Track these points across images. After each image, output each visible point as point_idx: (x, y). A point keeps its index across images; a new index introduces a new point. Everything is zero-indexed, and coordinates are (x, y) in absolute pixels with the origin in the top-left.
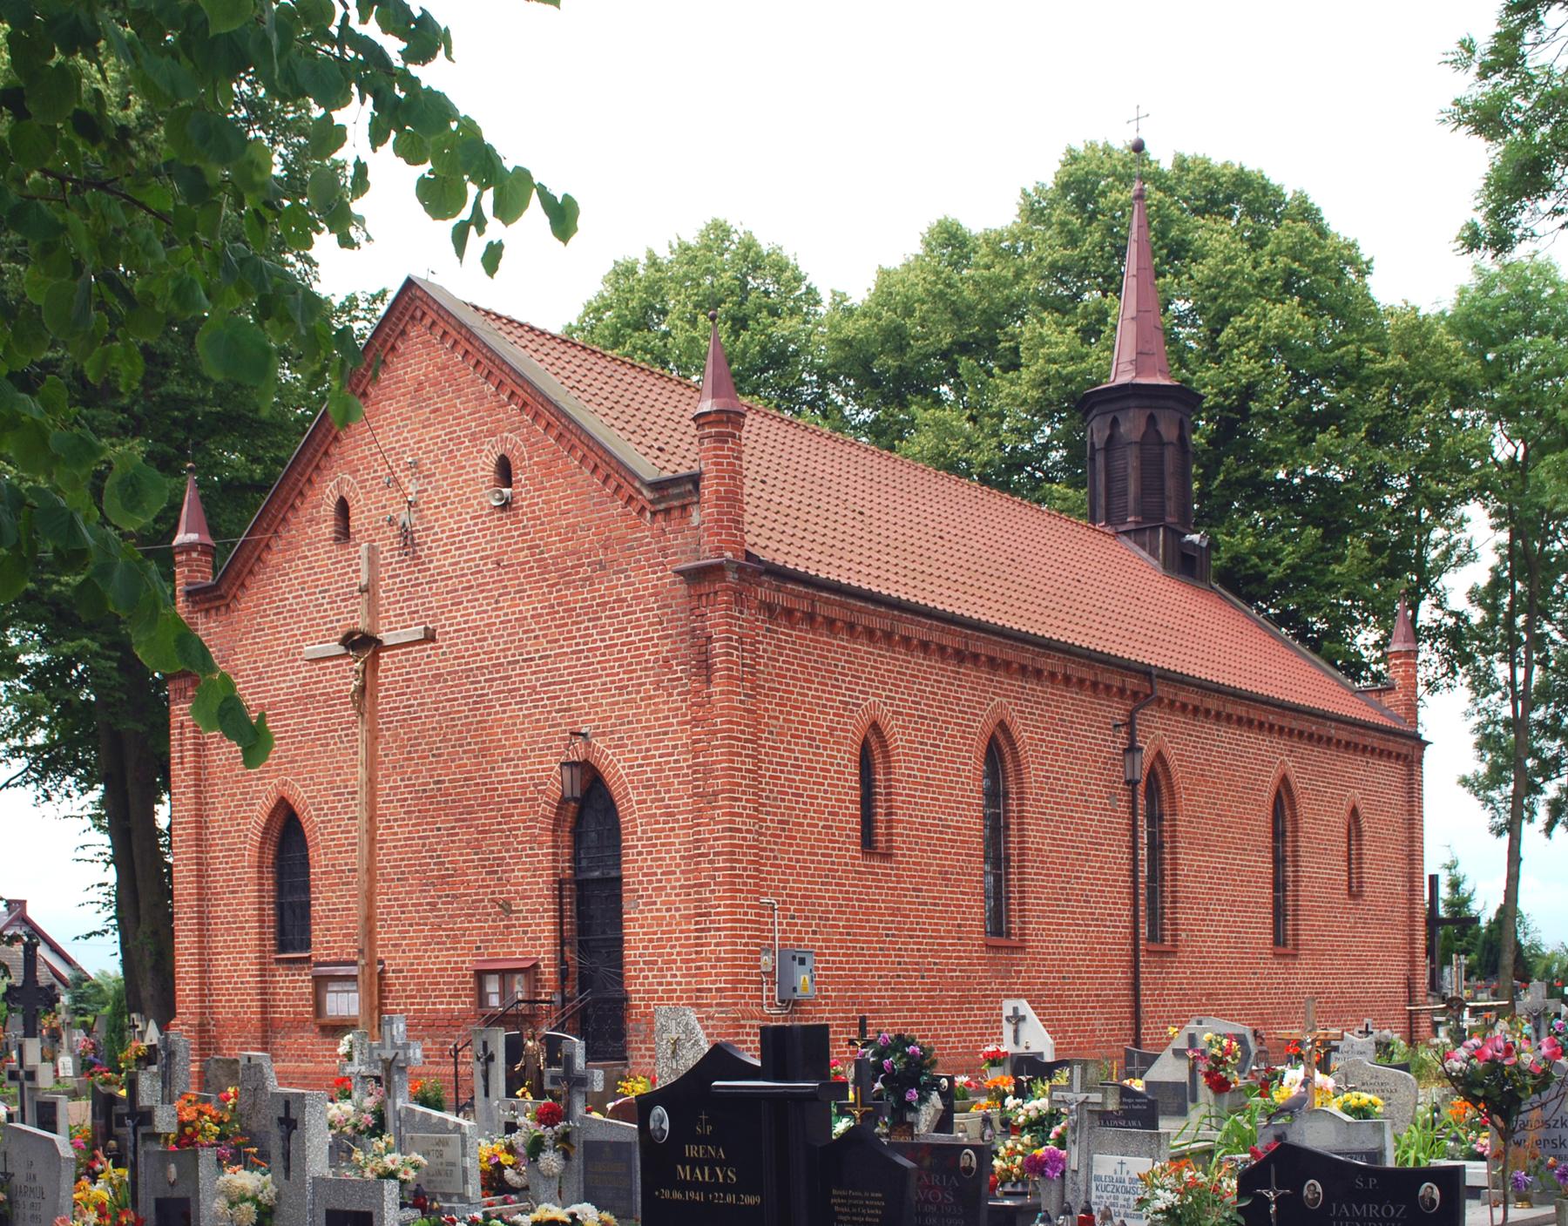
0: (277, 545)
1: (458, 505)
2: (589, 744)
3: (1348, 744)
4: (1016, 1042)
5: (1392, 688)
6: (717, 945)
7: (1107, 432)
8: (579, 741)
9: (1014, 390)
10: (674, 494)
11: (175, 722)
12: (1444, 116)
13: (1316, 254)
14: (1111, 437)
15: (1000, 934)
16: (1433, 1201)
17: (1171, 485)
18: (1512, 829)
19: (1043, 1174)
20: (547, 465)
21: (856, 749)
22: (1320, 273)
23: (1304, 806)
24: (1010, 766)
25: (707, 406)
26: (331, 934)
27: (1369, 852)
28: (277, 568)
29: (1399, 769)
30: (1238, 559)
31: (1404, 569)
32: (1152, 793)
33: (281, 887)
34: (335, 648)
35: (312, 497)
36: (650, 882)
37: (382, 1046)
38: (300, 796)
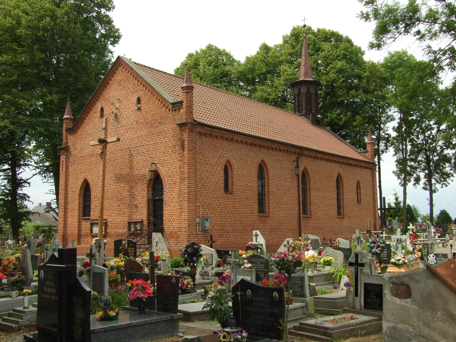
0: (87, 118)
1: (128, 110)
2: (156, 166)
3: (356, 165)
4: (256, 241)
5: (368, 152)
6: (185, 216)
7: (298, 92)
8: (154, 166)
9: (279, 82)
10: (177, 106)
11: (61, 160)
12: (357, 16)
13: (350, 50)
14: (299, 93)
15: (263, 213)
16: (276, 297)
17: (313, 104)
18: (404, 185)
19: (225, 280)
20: (148, 99)
21: (223, 167)
22: (352, 54)
23: (345, 180)
24: (265, 171)
25: (184, 85)
26: (95, 214)
27: (362, 191)
28: (87, 124)
29: (369, 171)
30: (332, 120)
31: (375, 123)
32: (304, 179)
33: (85, 201)
34: (96, 143)
35: (95, 107)
36: (170, 200)
37: (53, 245)
38: (89, 179)
